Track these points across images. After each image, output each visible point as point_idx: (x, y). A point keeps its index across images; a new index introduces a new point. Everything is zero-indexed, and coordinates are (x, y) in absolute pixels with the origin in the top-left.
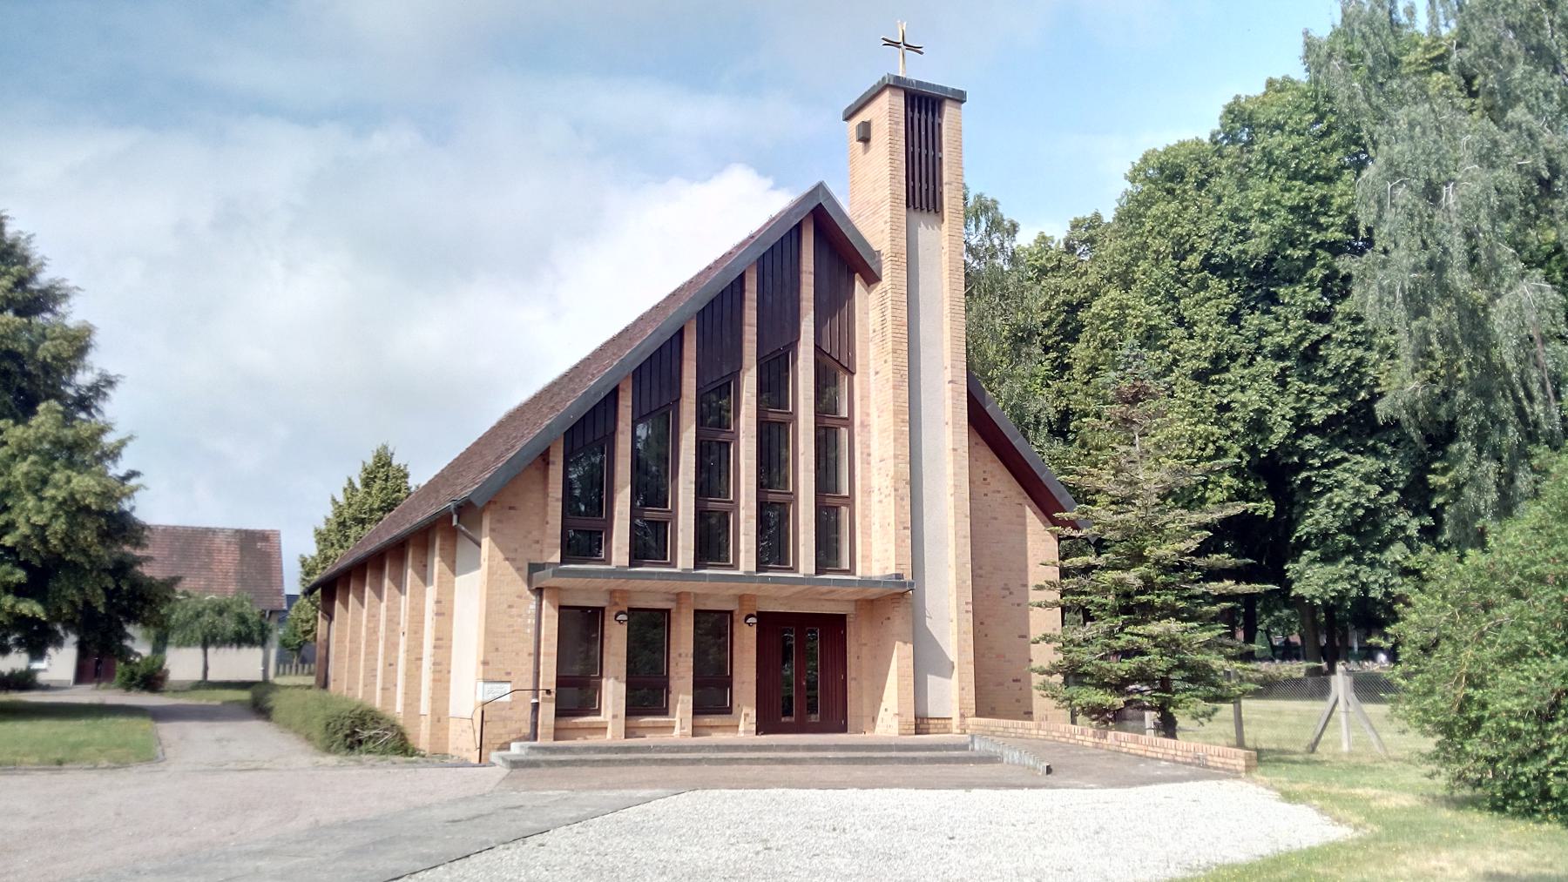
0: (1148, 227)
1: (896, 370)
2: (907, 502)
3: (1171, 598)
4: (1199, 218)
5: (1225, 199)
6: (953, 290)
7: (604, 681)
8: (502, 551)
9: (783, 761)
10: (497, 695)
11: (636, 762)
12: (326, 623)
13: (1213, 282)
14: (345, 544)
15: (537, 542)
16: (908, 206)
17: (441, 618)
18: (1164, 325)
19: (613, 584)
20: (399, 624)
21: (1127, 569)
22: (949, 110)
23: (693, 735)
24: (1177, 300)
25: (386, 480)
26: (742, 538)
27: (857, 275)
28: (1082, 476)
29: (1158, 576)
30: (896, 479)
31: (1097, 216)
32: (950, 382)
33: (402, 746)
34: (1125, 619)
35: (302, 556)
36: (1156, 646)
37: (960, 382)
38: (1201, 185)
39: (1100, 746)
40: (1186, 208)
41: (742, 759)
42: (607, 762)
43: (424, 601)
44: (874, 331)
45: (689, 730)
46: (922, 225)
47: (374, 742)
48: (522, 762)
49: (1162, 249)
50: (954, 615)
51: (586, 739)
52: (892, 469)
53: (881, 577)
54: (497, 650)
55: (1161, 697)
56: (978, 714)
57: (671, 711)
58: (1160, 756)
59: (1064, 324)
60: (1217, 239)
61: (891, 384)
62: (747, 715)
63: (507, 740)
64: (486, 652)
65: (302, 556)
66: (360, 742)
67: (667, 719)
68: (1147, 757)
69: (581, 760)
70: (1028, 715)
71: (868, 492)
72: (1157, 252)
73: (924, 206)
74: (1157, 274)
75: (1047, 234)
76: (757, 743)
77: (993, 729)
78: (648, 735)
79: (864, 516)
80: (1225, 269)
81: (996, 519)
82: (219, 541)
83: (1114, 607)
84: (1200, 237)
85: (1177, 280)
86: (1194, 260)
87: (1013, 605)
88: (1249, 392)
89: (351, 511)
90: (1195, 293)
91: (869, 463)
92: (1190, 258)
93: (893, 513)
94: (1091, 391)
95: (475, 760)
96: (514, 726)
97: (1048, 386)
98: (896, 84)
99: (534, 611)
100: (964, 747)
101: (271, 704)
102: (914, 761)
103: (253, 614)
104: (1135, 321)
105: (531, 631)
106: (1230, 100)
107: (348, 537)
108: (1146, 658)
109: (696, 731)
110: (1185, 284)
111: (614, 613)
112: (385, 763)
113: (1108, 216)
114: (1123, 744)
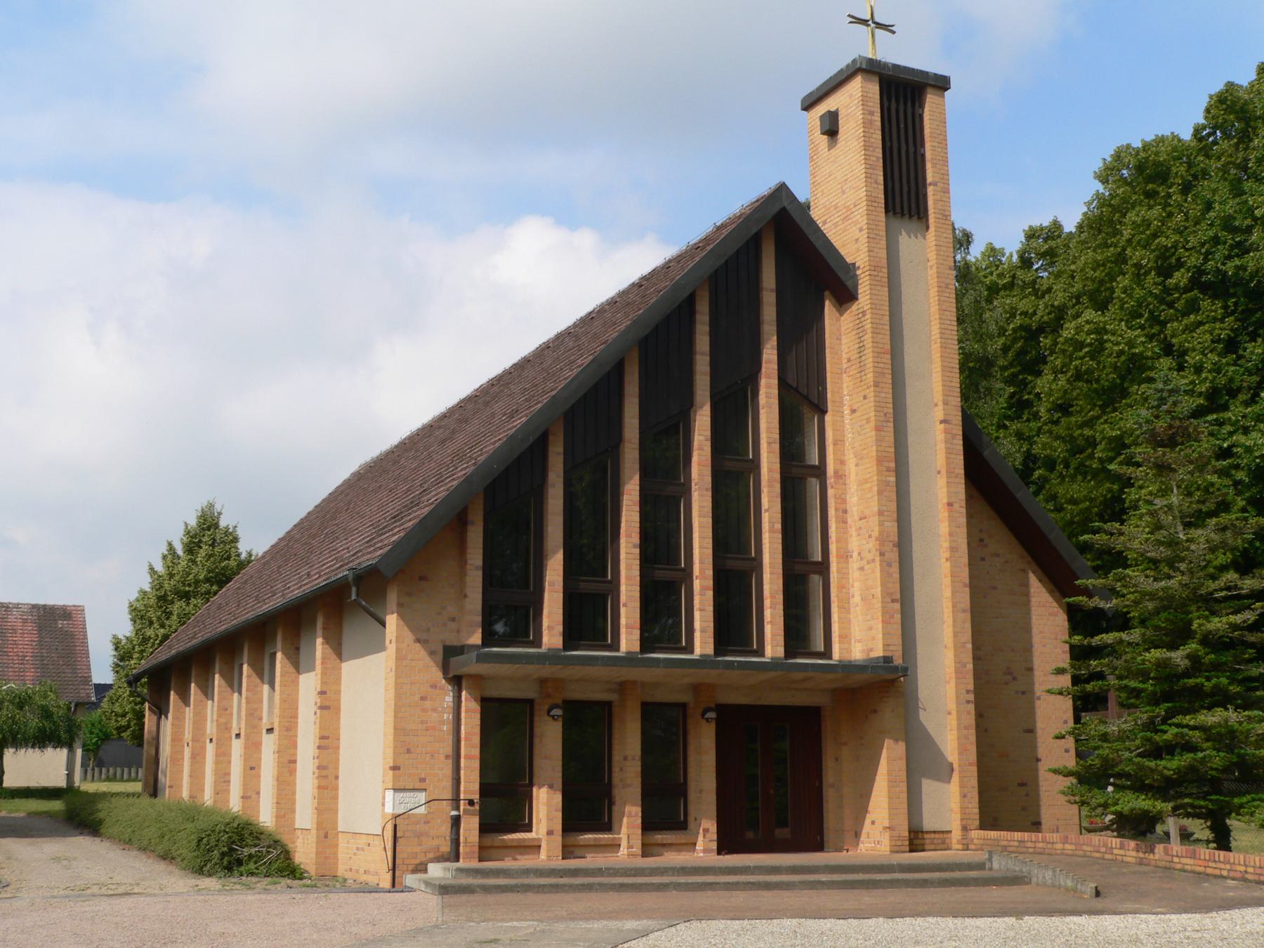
0: (1127, 233)
1: (878, 408)
2: (895, 570)
3: (1224, 681)
4: (1186, 228)
5: (1217, 206)
6: (942, 311)
7: (535, 790)
8: (411, 631)
9: (768, 886)
10: (410, 806)
11: (589, 888)
12: (155, 718)
13: (1205, 304)
14: (167, 623)
15: (453, 620)
16: (887, 211)
17: (326, 712)
18: (1150, 354)
19: (547, 671)
20: (261, 719)
21: (1173, 647)
22: (931, 99)
23: (644, 855)
24: (1163, 324)
25: (213, 545)
26: (697, 615)
27: (827, 293)
28: (1112, 534)
29: (1207, 654)
30: (882, 540)
31: (1056, 225)
32: (941, 422)
33: (287, 869)
34: (1169, 708)
35: (115, 637)
36: (1207, 740)
37: (954, 422)
38: (1186, 189)
39: (1145, 861)
40: (1170, 215)
41: (716, 884)
42: (556, 888)
43: (297, 691)
44: (849, 360)
45: (637, 849)
46: (903, 233)
47: (255, 863)
48: (452, 887)
49: (1144, 262)
50: (952, 706)
51: (515, 859)
52: (877, 529)
53: (864, 660)
54: (409, 751)
55: (1217, 800)
56: (983, 826)
57: (615, 826)
58: (1225, 873)
59: (1022, 352)
60: (1208, 253)
61: (872, 424)
62: (706, 831)
63: (424, 859)
64: (396, 754)
65: (115, 637)
66: (239, 862)
67: (611, 836)
68: (1207, 875)
69: (523, 885)
70: (1036, 826)
71: (845, 556)
72: (1138, 266)
73: (906, 211)
74: (1138, 293)
75: (997, 246)
76: (721, 864)
77: (1005, 843)
78: (589, 856)
79: (841, 587)
80: (1219, 287)
81: (994, 588)
82: (13, 617)
83: (1154, 693)
84: (1187, 250)
85: (1162, 301)
86: (1180, 278)
87: (1017, 692)
88: (1254, 435)
89: (172, 583)
90: (1183, 316)
91: (845, 522)
92: (1177, 274)
93: (879, 583)
94: (1062, 432)
95: (386, 883)
96: (430, 843)
97: (1005, 427)
98: (870, 68)
99: (451, 704)
100: (980, 866)
101: (101, 815)
102: (924, 884)
103: (59, 707)
104: (1116, 348)
105: (447, 728)
106: (1218, 87)
107: (171, 613)
108: (1200, 755)
109: (647, 851)
110: (1171, 305)
111: (546, 707)
112: (279, 887)
113: (1070, 226)
114: (1176, 860)
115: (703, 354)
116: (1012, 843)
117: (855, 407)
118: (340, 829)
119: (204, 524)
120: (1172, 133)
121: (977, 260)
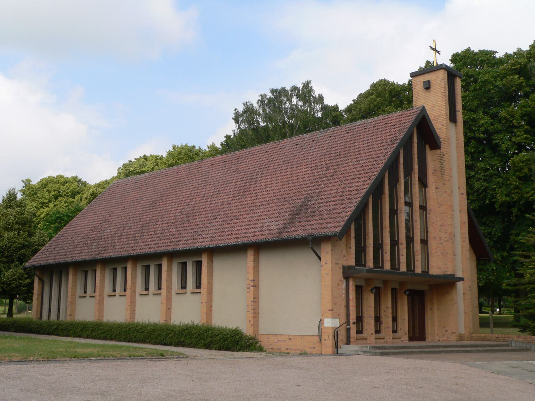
115: (402, 164)
116: (493, 338)
117: (438, 187)
118: (259, 333)
119: (10, 197)
120: (385, 79)
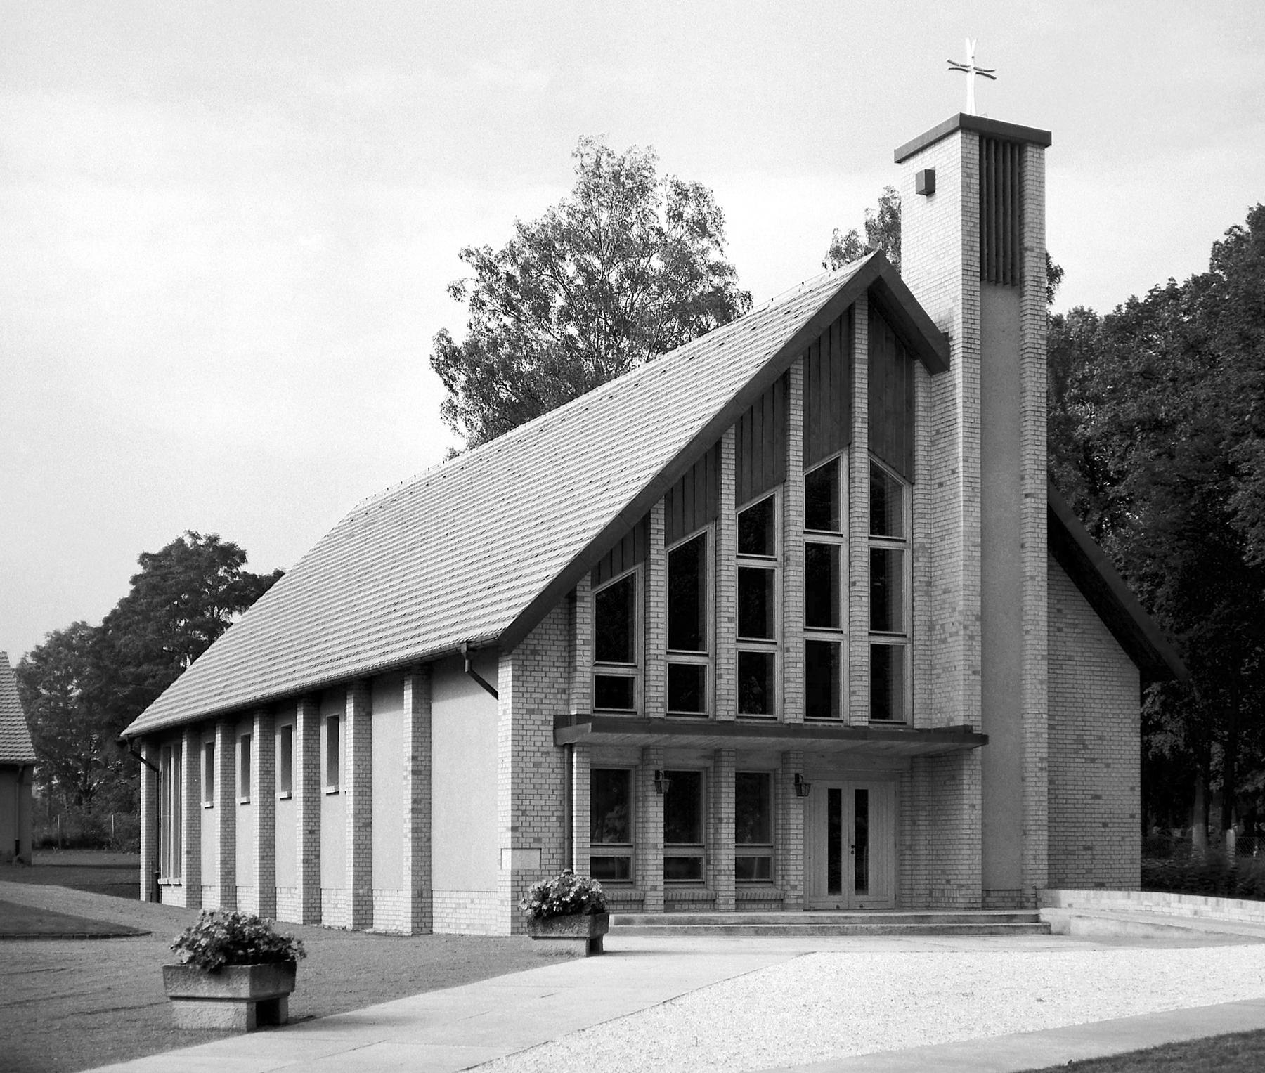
16: (982, 279)
22: (1030, 152)
98: (967, 124)
121: (572, 212)
